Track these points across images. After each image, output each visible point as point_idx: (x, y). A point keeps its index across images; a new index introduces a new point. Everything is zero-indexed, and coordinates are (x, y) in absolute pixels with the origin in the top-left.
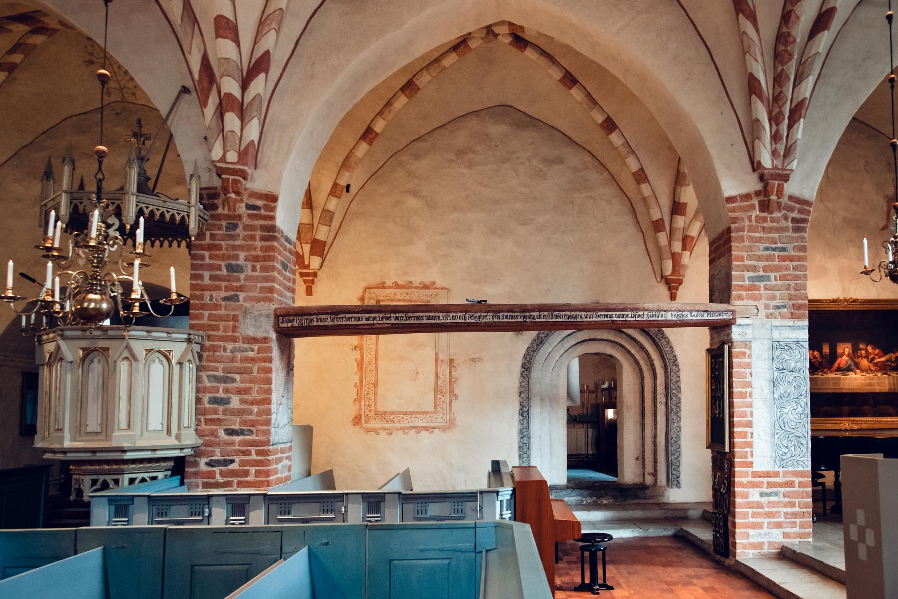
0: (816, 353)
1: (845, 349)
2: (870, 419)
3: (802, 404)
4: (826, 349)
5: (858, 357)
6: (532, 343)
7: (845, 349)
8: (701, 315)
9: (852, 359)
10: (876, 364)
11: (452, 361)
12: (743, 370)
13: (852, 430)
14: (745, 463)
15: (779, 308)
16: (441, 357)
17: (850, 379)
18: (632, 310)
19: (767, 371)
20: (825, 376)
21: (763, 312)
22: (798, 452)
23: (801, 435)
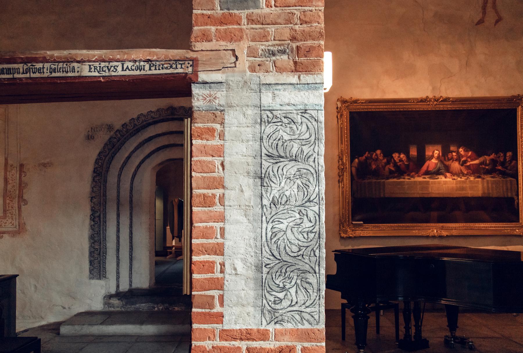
0: (402, 156)
1: (434, 152)
2: (461, 225)
3: (311, 214)
4: (413, 152)
5: (449, 160)
6: (104, 148)
7: (434, 152)
8: (139, 68)
9: (442, 162)
10: (468, 167)
11: (22, 166)
12: (210, 159)
13: (441, 237)
14: (209, 314)
15: (274, 55)
16: (10, 162)
17: (439, 183)
18: (25, 61)
19: (250, 160)
20: (412, 180)
21: (244, 62)
22: (302, 297)
23: (307, 267)
